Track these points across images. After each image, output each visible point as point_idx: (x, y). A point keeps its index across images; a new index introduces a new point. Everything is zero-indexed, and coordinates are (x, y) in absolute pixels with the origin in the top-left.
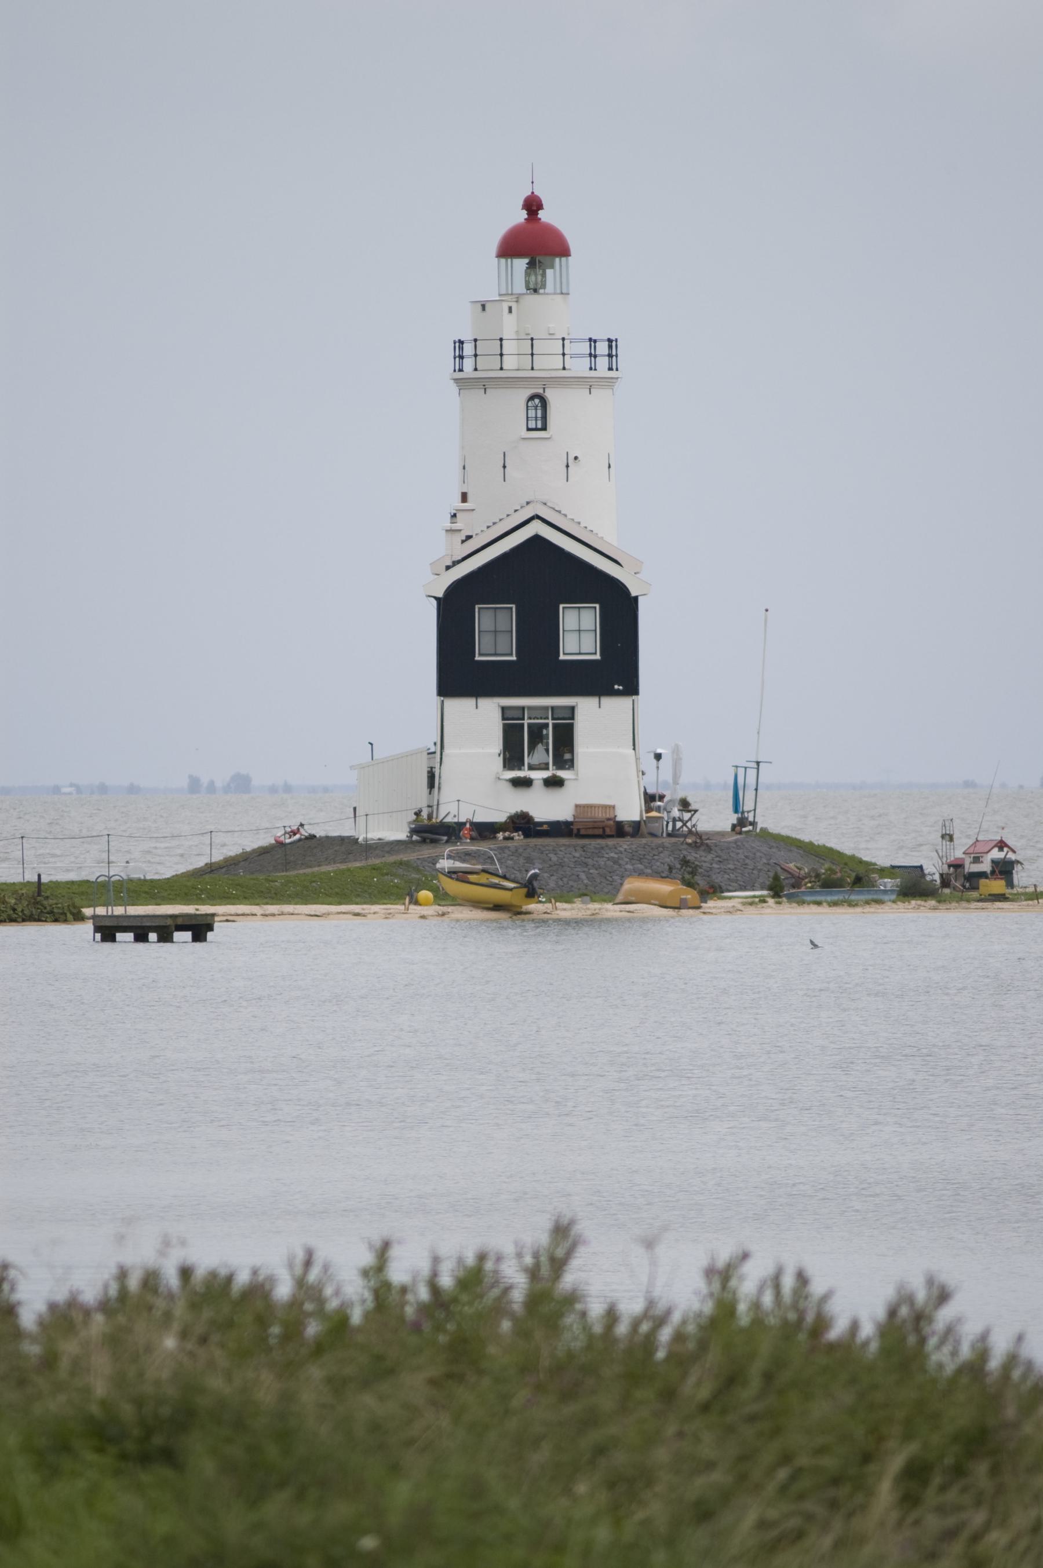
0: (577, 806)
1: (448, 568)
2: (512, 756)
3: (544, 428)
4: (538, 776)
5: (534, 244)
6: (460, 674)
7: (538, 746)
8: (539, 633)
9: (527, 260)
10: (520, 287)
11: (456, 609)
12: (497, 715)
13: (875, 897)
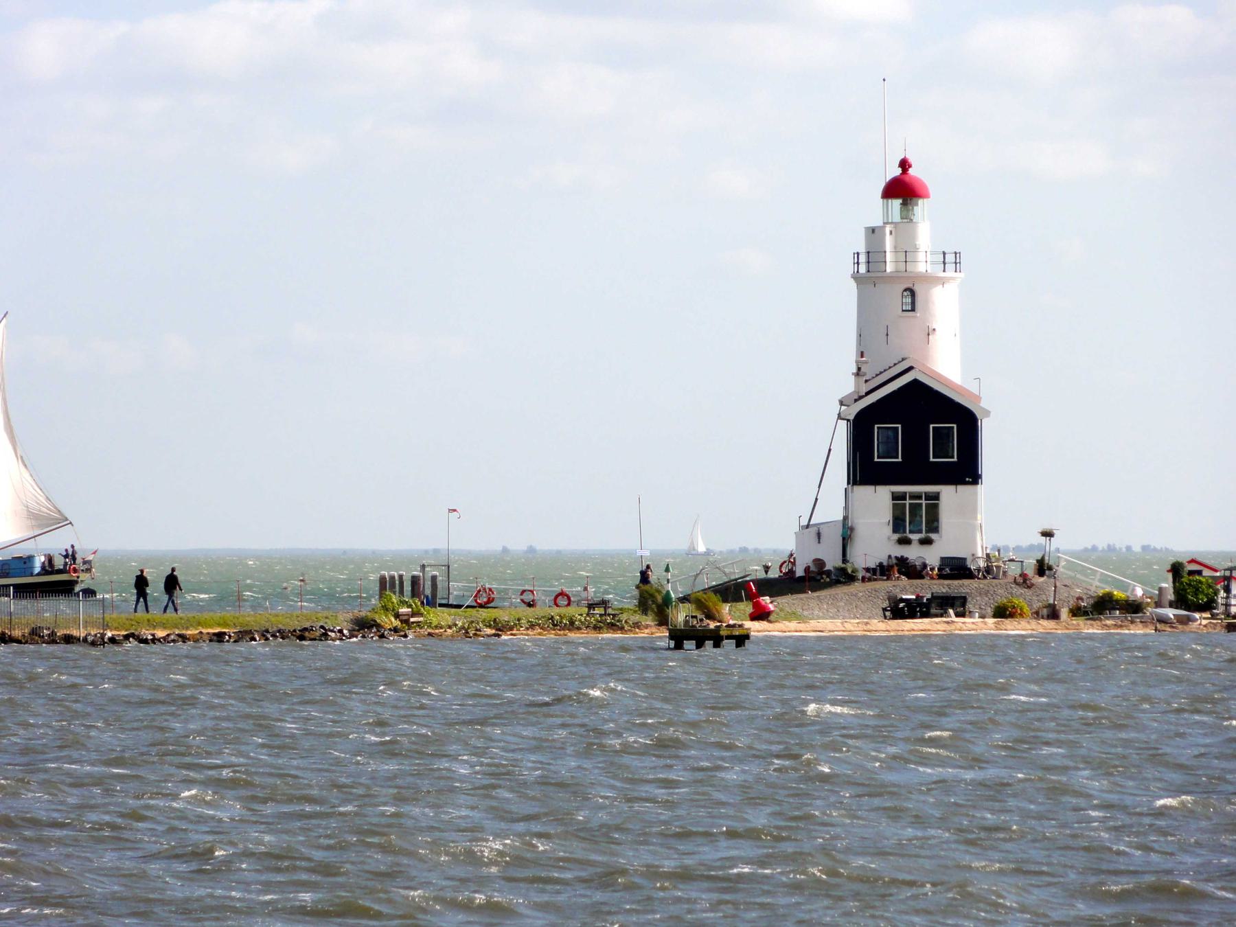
0: (942, 559)
1: (856, 401)
2: (898, 524)
3: (913, 310)
4: (915, 537)
5: (902, 189)
6: (864, 471)
7: (915, 520)
8: (915, 443)
9: (900, 201)
10: (897, 218)
11: (862, 427)
12: (889, 496)
13: (510, 755)
